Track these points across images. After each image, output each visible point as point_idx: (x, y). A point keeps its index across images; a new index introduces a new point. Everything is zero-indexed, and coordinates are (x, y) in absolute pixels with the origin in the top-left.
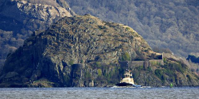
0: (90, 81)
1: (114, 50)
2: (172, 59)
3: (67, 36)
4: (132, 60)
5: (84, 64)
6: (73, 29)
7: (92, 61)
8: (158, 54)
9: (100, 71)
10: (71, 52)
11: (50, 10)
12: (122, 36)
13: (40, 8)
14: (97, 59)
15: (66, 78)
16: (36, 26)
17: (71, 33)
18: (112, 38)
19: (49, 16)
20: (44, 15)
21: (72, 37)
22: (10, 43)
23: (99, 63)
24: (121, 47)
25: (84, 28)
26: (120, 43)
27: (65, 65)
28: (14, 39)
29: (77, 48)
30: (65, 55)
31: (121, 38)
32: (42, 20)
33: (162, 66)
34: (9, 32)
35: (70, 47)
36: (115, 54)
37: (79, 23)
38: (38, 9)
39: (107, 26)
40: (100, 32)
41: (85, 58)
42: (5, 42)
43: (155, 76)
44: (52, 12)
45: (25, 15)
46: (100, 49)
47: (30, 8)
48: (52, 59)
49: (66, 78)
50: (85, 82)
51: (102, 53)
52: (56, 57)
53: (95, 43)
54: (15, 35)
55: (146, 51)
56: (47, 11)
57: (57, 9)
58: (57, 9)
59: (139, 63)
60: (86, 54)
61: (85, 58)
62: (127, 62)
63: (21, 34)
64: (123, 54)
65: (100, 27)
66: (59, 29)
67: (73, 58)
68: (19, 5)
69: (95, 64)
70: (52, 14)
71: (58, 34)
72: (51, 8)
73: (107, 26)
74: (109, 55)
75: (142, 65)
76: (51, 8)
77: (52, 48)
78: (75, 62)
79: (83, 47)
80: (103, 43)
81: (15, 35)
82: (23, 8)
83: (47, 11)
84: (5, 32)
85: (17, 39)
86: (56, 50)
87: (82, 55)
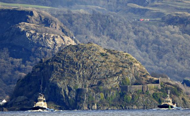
0: (93, 104)
1: (115, 75)
2: (168, 84)
3: (72, 62)
4: (132, 85)
5: (87, 89)
6: (77, 57)
7: (95, 85)
8: (155, 79)
9: (102, 95)
10: (76, 78)
11: (56, 39)
12: (123, 62)
13: (47, 37)
14: (100, 83)
15: (71, 101)
16: (43, 54)
17: (76, 60)
18: (113, 64)
19: (55, 45)
20: (50, 43)
21: (77, 64)
22: (20, 69)
23: (101, 87)
24: (121, 72)
25: (87, 55)
26: (121, 69)
27: (70, 89)
28: (23, 66)
29: (81, 73)
30: (70, 80)
31: (121, 64)
32: (49, 48)
33: (159, 90)
34: (18, 60)
35: (75, 73)
36: (116, 79)
37: (82, 51)
38: (45, 38)
39: (108, 53)
40: (102, 59)
41: (88, 83)
42: (15, 69)
43: (154, 100)
44: (58, 40)
45: (33, 43)
46: (102, 74)
47: (38, 37)
48: (58, 84)
49: (71, 101)
50: (89, 105)
51: (104, 78)
52: (62, 82)
53: (97, 69)
54: (24, 62)
55: (144, 76)
56: (54, 40)
57: (63, 38)
58: (63, 38)
59: (138, 87)
60: (89, 79)
61: (88, 83)
62: (127, 87)
63: (30, 61)
64: (124, 79)
65: (102, 54)
66: (65, 56)
67: (78, 83)
68: (28, 35)
69: (98, 88)
70: (58, 42)
71: (63, 61)
72: (57, 37)
73: (108, 53)
74: (111, 80)
75: (141, 89)
76: (57, 37)
77: (58, 74)
78: (80, 86)
79: (87, 73)
80: (105, 69)
81: (24, 62)
82: (31, 37)
83: (54, 40)
84: (15, 60)
85: (26, 66)
86: (62, 76)
87: (85, 80)
